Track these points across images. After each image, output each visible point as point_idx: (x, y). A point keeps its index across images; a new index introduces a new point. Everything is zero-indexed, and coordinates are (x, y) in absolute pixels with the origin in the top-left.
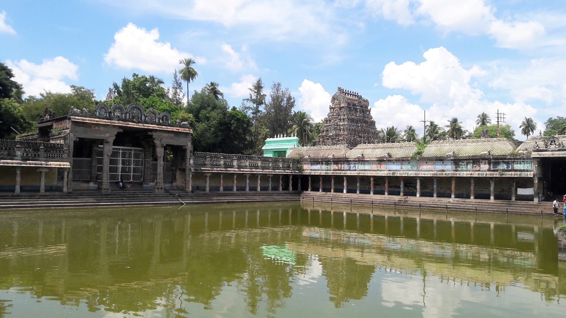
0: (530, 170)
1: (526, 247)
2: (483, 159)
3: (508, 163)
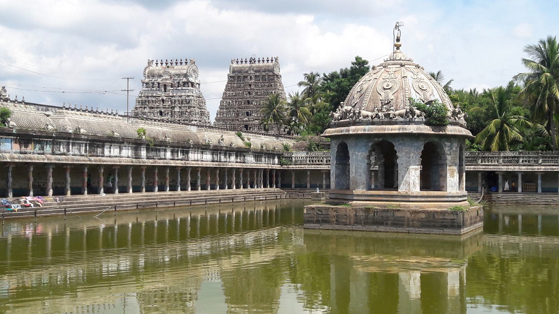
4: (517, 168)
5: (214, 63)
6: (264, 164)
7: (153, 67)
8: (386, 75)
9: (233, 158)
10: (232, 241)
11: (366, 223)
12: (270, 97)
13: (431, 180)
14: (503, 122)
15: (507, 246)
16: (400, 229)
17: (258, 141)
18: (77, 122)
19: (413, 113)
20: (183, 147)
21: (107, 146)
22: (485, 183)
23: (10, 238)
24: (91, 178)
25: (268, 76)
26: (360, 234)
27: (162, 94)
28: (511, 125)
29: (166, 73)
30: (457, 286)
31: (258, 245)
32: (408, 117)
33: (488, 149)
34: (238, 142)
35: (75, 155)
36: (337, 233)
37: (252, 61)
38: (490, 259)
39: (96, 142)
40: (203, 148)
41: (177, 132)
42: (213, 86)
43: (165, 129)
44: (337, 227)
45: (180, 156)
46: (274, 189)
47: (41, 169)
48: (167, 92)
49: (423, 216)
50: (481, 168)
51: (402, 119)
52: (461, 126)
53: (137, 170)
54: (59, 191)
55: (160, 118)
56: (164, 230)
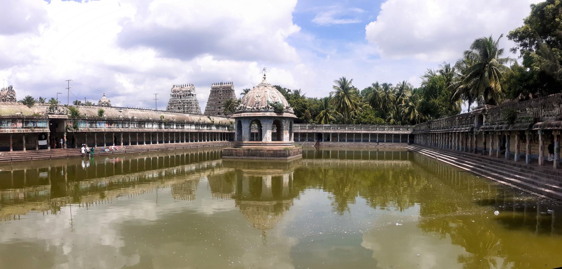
0: (44, 127)
1: (44, 182)
2: (19, 119)
3: (34, 122)
4: (330, 131)
5: (202, 84)
6: (221, 130)
7: (175, 88)
8: (258, 91)
9: (205, 128)
10: (206, 164)
11: (248, 156)
12: (228, 100)
13: (277, 136)
14: (326, 112)
15: (325, 164)
16: (262, 158)
17: (217, 120)
18: (133, 114)
19: (269, 108)
20: (181, 123)
21: (146, 124)
22: (299, 137)
23: (105, 162)
24: (150, 137)
25: (229, 91)
26: (245, 160)
27: (180, 100)
28: (330, 113)
29: (181, 90)
30: (288, 181)
31: (218, 166)
32: (266, 109)
33: (320, 123)
34: (208, 121)
35: (133, 128)
36: (236, 160)
37: (221, 83)
38: (320, 170)
39: (141, 122)
40: (191, 123)
41: (179, 116)
42: (203, 96)
43: (173, 116)
44: (236, 157)
45: (180, 127)
46: (226, 141)
47: (118, 134)
48: (181, 100)
49: (272, 152)
50: (315, 131)
51: (263, 110)
52: (291, 113)
53: (160, 134)
54: (126, 144)
55: (178, 111)
56: (184, 159)
